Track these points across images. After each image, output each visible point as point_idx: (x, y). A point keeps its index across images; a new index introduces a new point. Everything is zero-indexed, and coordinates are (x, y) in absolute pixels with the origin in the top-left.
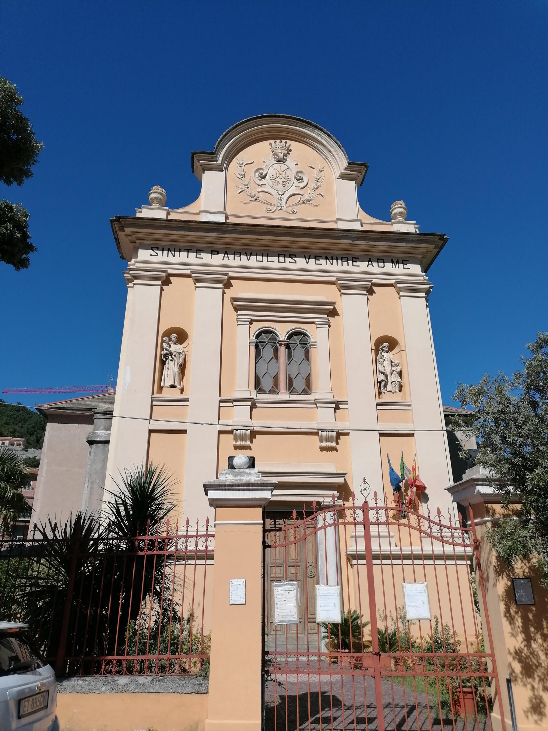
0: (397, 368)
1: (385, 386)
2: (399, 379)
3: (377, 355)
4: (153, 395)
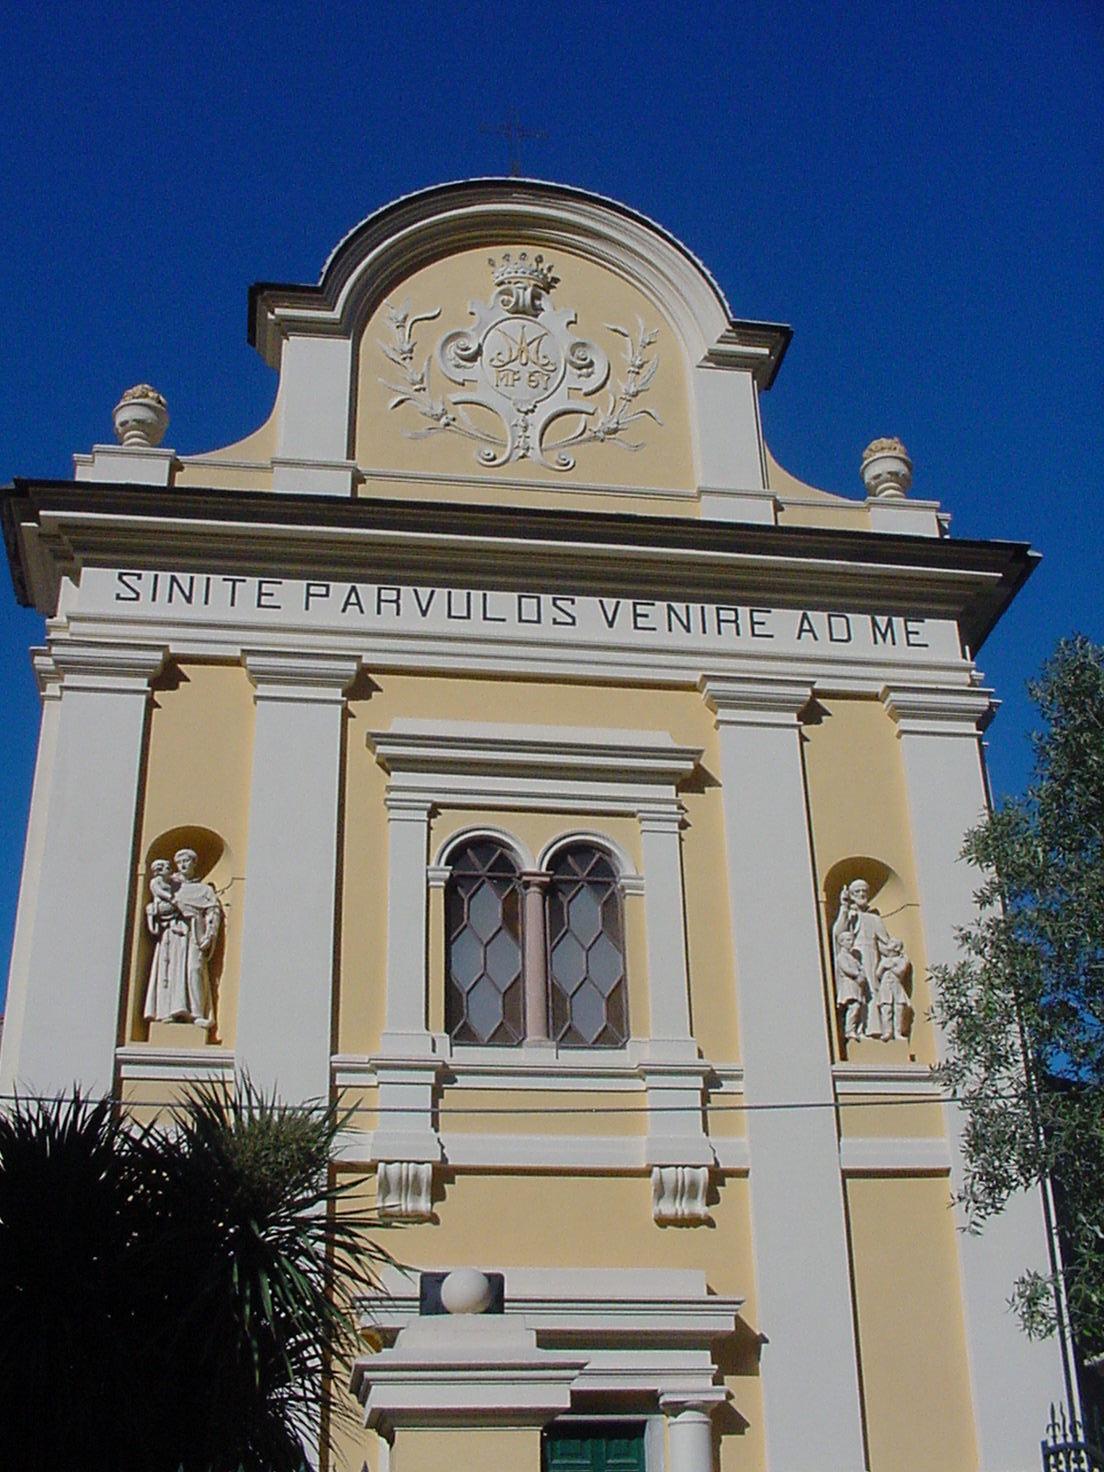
0: (896, 959)
1: (861, 1018)
2: (902, 997)
3: (832, 918)
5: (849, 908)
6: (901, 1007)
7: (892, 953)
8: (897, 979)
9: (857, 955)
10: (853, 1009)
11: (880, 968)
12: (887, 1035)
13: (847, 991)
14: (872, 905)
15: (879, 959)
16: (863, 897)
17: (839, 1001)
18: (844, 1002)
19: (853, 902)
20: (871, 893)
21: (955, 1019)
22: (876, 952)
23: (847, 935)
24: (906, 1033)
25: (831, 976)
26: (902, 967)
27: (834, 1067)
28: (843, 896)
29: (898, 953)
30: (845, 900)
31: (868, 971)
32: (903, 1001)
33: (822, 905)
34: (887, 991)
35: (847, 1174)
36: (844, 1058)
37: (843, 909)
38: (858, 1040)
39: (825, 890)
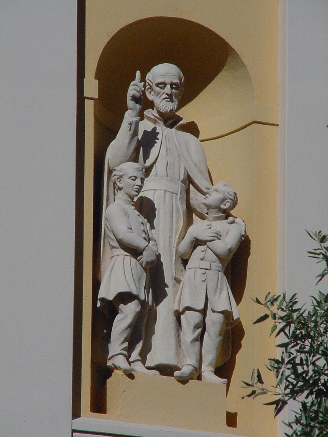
0: (221, 225)
1: (141, 331)
2: (223, 299)
3: (107, 133)
4: (76, 413)
5: (141, 116)
6: (220, 318)
7: (213, 214)
8: (217, 265)
9: (146, 208)
10: (127, 314)
11: (188, 239)
12: (186, 370)
13: (120, 275)
14: (187, 114)
15: (189, 222)
16: (170, 97)
17: (101, 294)
18: (111, 298)
19: (150, 105)
20: (186, 92)
21: (301, 398)
22: (182, 208)
23: (130, 169)
24: (224, 370)
25: (90, 239)
26: (228, 242)
27: (78, 423)
28: (133, 90)
29: (227, 214)
30: (135, 99)
31: (165, 238)
32: (226, 307)
33: (89, 107)
34: (197, 285)
35: (74, 431)
36: (99, 405)
37: (129, 117)
38: (131, 376)
39: (98, 76)
